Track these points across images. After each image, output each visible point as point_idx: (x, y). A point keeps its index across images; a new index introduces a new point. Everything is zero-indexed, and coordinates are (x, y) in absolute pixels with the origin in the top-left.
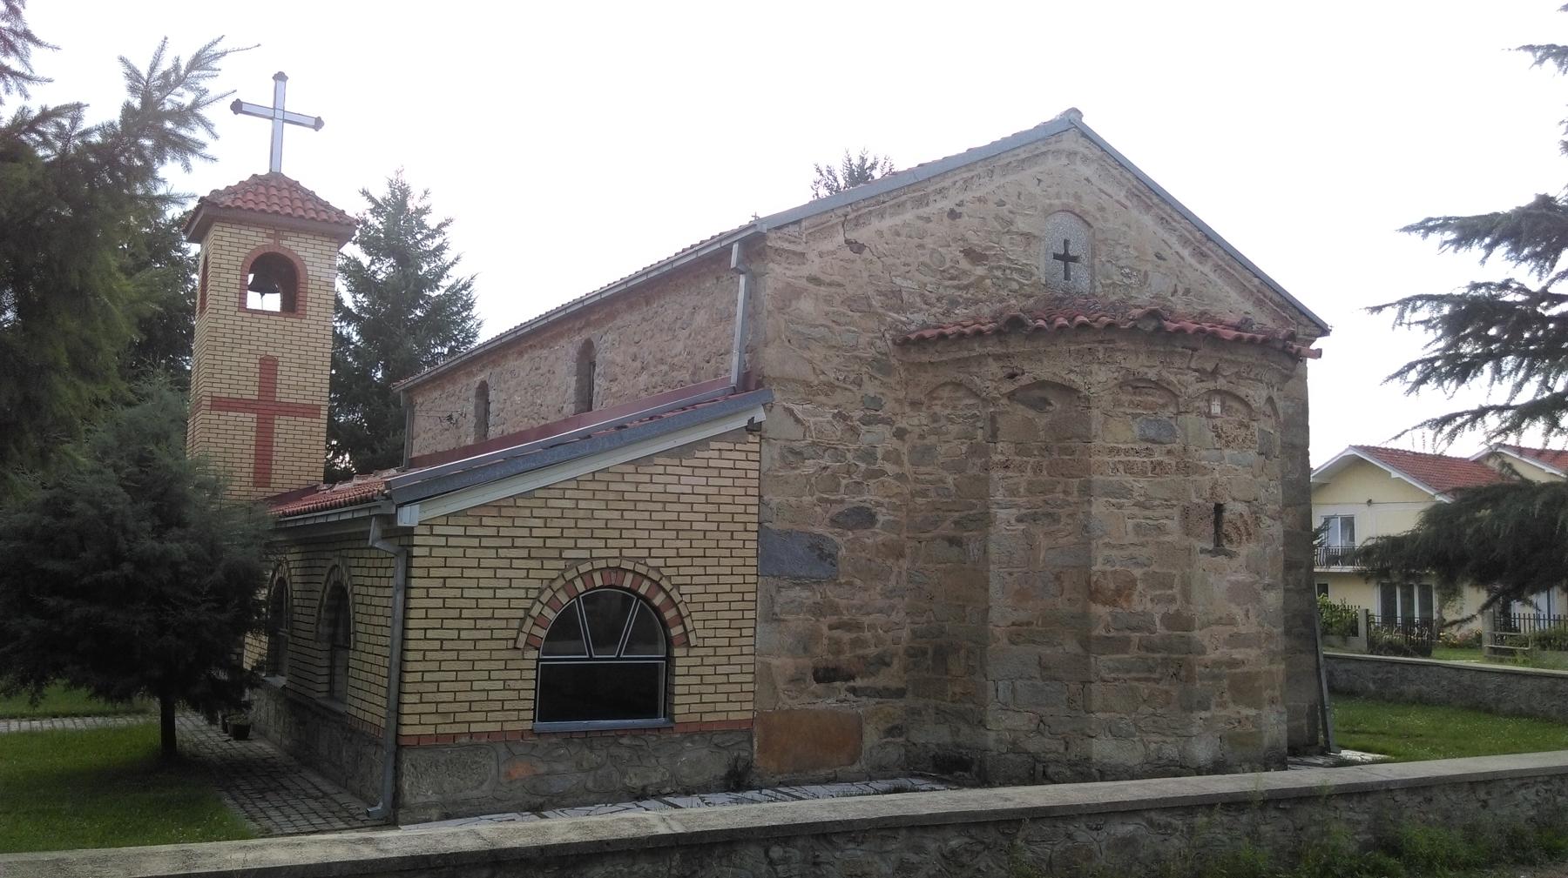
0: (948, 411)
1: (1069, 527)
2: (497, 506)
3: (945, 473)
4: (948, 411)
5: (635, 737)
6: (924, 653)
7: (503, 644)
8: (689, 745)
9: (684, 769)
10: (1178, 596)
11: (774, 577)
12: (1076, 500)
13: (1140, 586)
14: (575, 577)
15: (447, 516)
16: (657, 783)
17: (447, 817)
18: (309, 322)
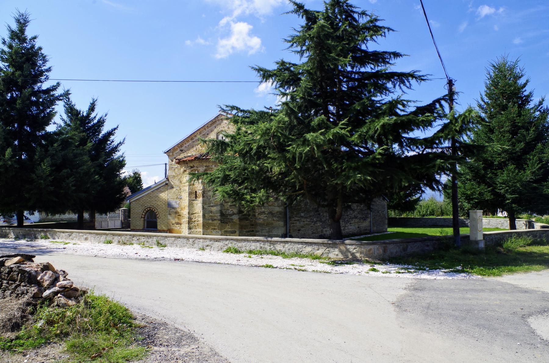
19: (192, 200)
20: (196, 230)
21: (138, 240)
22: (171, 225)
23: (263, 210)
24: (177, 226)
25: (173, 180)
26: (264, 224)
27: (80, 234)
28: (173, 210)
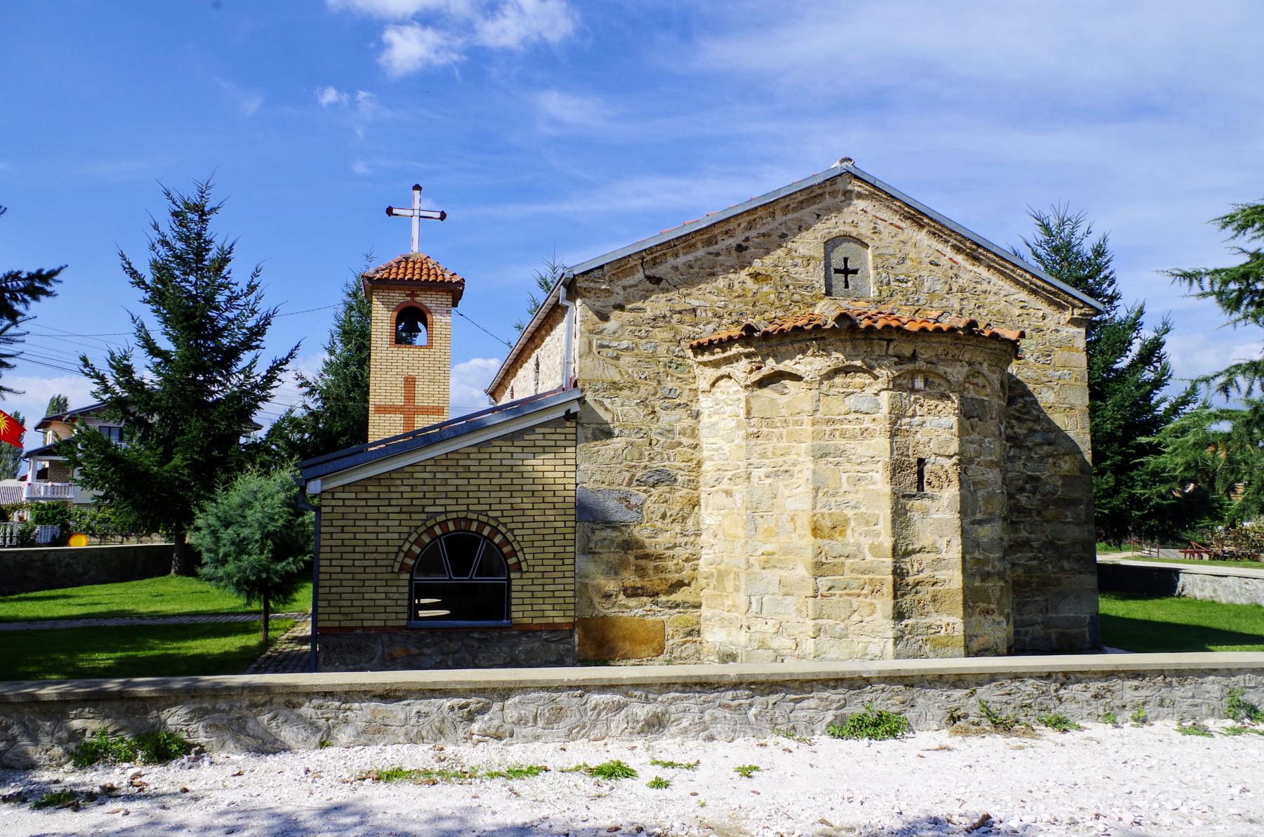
2: (377, 479)
4: (724, 396)
5: (482, 632)
13: (852, 524)
19: (904, 496)
20: (928, 620)
21: (1095, 697)
22: (596, 599)
23: (1024, 534)
24: (632, 602)
25: (607, 402)
26: (1029, 583)
27: (595, 698)
28: (608, 533)
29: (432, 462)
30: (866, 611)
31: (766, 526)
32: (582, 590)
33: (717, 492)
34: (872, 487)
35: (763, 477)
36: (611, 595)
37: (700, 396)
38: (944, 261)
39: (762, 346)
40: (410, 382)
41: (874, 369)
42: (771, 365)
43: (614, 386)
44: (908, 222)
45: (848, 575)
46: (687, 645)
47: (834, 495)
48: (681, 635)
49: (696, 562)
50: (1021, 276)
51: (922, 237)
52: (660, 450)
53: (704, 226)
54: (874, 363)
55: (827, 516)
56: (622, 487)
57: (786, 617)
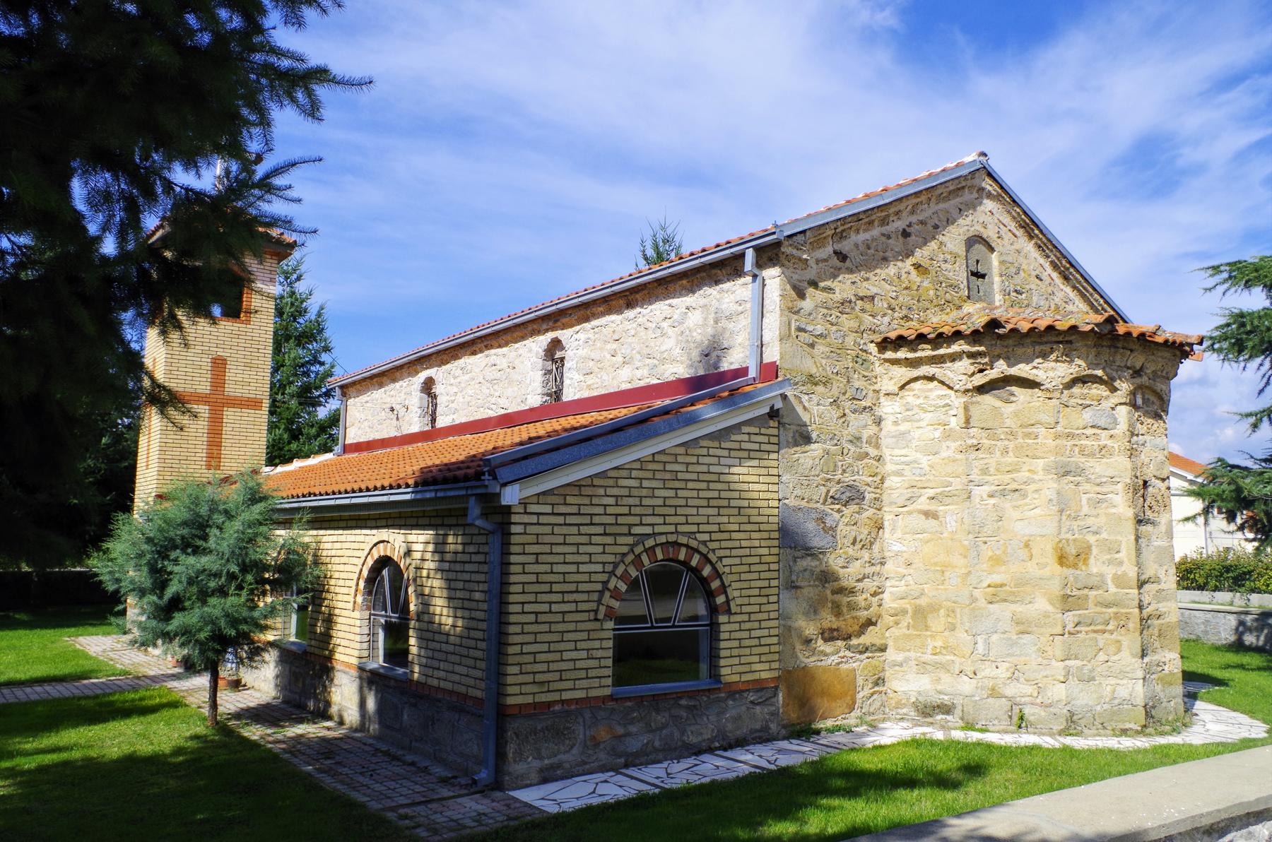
0: (921, 401)
1: (1035, 501)
2: (577, 485)
3: (918, 455)
4: (921, 401)
5: (690, 698)
6: (904, 612)
7: (585, 616)
8: (731, 702)
9: (728, 725)
10: (1125, 559)
11: (791, 548)
12: (1040, 477)
13: (1095, 551)
14: (642, 552)
15: (538, 495)
16: (708, 739)
17: (545, 781)
18: (253, 327)
29: (637, 465)
30: (1112, 649)
31: (990, 553)
32: (787, 634)
33: (910, 513)
34: (1113, 510)
35: (985, 497)
36: (811, 640)
37: (882, 399)
38: (1044, 276)
39: (996, 345)
40: (219, 365)
41: (1115, 381)
42: (1000, 368)
43: (812, 380)
44: (1022, 230)
45: (1093, 610)
46: (875, 696)
47: (1075, 519)
48: (870, 686)
49: (881, 596)
50: (1097, 301)
51: (1029, 247)
52: (850, 461)
53: (887, 201)
54: (1114, 374)
55: (1071, 543)
56: (818, 505)
57: (1022, 659)
